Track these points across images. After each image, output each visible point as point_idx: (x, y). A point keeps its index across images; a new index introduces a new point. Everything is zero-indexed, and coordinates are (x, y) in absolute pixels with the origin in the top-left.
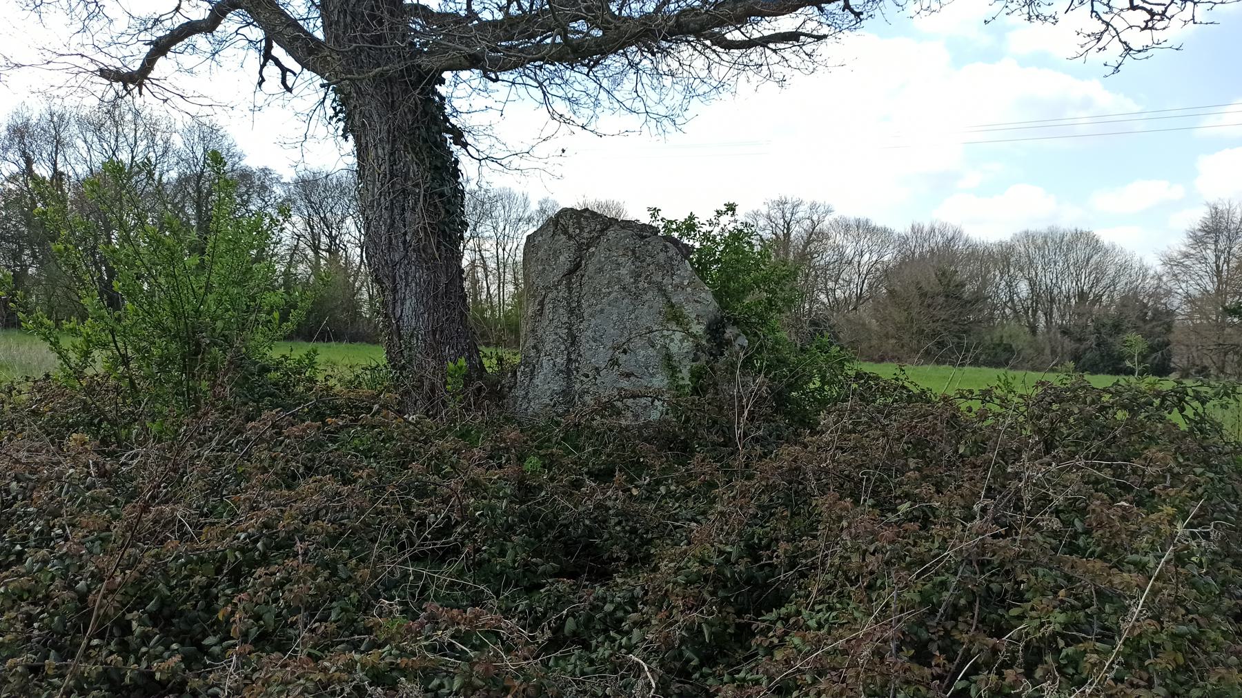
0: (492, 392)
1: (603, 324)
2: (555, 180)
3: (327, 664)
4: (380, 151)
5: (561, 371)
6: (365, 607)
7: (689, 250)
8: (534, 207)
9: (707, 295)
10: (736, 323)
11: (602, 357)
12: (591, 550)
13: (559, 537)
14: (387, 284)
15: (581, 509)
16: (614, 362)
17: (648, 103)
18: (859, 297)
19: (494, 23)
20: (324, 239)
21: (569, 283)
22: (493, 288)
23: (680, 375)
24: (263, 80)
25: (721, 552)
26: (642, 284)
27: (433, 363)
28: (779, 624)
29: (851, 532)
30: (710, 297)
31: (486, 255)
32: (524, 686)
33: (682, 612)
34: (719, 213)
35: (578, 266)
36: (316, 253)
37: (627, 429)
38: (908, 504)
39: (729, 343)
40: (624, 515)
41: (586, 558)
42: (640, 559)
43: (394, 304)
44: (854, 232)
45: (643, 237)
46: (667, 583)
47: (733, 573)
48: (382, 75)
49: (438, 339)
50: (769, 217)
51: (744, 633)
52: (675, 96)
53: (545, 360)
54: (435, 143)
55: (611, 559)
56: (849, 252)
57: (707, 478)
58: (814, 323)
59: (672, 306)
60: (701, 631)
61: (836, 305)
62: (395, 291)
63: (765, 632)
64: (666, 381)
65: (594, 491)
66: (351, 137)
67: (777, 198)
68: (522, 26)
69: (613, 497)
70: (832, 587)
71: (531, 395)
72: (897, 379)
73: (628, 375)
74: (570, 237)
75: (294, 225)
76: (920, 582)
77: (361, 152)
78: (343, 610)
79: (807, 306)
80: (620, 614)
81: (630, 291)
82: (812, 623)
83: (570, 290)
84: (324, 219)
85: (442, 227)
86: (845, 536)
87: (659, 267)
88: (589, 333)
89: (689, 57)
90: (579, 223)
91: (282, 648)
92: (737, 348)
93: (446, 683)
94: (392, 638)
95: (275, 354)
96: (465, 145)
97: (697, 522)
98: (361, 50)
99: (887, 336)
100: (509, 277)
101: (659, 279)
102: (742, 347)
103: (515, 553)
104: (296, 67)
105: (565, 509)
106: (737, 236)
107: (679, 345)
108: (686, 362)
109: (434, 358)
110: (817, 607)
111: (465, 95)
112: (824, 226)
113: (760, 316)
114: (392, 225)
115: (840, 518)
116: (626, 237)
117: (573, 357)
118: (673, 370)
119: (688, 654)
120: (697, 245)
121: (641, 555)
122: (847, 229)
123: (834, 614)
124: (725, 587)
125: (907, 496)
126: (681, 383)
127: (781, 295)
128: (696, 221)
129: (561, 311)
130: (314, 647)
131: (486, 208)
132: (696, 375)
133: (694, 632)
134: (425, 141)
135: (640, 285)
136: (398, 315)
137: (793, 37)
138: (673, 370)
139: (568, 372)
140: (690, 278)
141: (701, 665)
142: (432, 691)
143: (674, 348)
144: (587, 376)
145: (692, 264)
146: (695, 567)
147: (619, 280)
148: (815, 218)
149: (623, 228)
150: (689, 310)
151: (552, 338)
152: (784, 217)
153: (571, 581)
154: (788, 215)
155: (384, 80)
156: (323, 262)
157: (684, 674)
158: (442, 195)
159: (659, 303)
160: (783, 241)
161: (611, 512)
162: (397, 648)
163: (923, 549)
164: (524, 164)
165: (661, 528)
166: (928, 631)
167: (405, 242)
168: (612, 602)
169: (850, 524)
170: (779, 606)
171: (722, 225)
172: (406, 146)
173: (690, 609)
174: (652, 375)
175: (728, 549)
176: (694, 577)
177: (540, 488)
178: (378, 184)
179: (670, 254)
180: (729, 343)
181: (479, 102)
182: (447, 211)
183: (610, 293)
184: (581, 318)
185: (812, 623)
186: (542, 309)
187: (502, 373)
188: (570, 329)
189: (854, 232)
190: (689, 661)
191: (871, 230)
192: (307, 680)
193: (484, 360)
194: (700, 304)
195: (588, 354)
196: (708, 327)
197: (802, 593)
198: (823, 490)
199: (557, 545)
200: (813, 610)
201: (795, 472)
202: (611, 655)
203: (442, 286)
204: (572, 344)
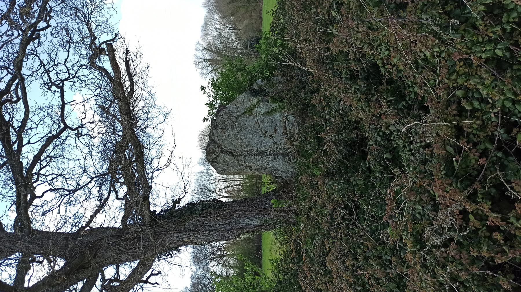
0: (284, 188)
1: (254, 141)
2: (192, 161)
3: (412, 263)
4: (185, 236)
5: (275, 158)
6: (384, 244)
7: (221, 105)
8: (203, 168)
9: (240, 97)
10: (252, 85)
11: (268, 141)
12: (353, 145)
13: (347, 159)
14: (240, 231)
15: (336, 151)
16: (271, 136)
17: (158, 122)
18: (235, 29)
19: (129, 188)
20: (219, 253)
21: (237, 156)
22: (236, 183)
23: (275, 108)
24: (156, 283)
25: (355, 92)
26: (237, 125)
27: (273, 211)
28: (387, 67)
29: (346, 37)
30: (241, 96)
31: (223, 186)
32: (419, 179)
33: (382, 109)
34: (205, 93)
35: (230, 152)
36: (225, 256)
37: (299, 131)
38: (333, 12)
39: (260, 87)
40: (339, 132)
41: (357, 148)
42: (357, 125)
43: (249, 228)
44: (207, 32)
45: (217, 125)
46: (369, 115)
47: (364, 87)
48: (154, 237)
49: (263, 210)
50: (202, 68)
51: (390, 82)
52: (154, 112)
53: (270, 165)
54: (181, 213)
55: (357, 137)
56: (215, 33)
57: (322, 98)
58: (246, 48)
59: (246, 112)
60: (390, 101)
61: (238, 39)
62: (243, 228)
63: (390, 73)
64: (278, 114)
65: (329, 146)
66: (180, 248)
67: (194, 65)
68: (129, 178)
69: (330, 137)
70: (370, 44)
71: (285, 170)
72: (273, 14)
73: (275, 130)
74: (218, 156)
75: (213, 266)
76: (368, 7)
77: (186, 244)
78: (386, 254)
79: (239, 51)
80: (381, 134)
81: (240, 130)
82: (387, 53)
83: (240, 155)
84: (211, 253)
85: (216, 210)
86: (350, 41)
87: (229, 118)
88: (258, 147)
89: (139, 106)
90: (212, 153)
91: (401, 278)
92: (262, 84)
93: (418, 211)
94: (398, 234)
95: (270, 275)
96: (180, 199)
97: (340, 101)
98: (143, 245)
99: (250, 16)
100: (232, 177)
101: (234, 118)
102: (262, 82)
103: (358, 180)
104: (151, 270)
105: (336, 158)
106: (214, 86)
107: (262, 109)
108: (269, 106)
109: (271, 211)
110: (379, 51)
111: (159, 202)
112: (204, 44)
113: (248, 74)
114: (216, 230)
115: (342, 42)
116: (217, 133)
117: (268, 153)
118: (273, 111)
119: (400, 106)
120: (219, 102)
121: (355, 125)
122: (206, 35)
123: (383, 44)
124: (369, 90)
125: (329, 12)
126: (278, 107)
127: (238, 66)
128: (208, 102)
129: (249, 159)
130: (403, 267)
131: (203, 189)
132: (274, 101)
133: (390, 104)
134: (180, 217)
135: (237, 126)
136: (253, 226)
137: (127, 63)
138: (273, 111)
139: (275, 155)
140: (233, 105)
141: (405, 100)
142: (422, 217)
143: (263, 111)
144: (277, 148)
145: (227, 104)
146: (362, 103)
147: (236, 135)
148: (202, 49)
149: (213, 134)
150: (247, 105)
151: (259, 162)
152: (202, 62)
153: (369, 156)
154: (201, 60)
155: (156, 235)
156: (228, 253)
157: (410, 108)
158: (202, 210)
159: (244, 117)
160: (212, 62)
161: (337, 138)
162: (403, 232)
163: (354, 6)
164: (186, 174)
165: (343, 117)
166: (391, 4)
167: (223, 225)
168: (377, 138)
169: (344, 39)
170: (379, 67)
171: (210, 91)
172: (182, 226)
173: (381, 105)
174: (275, 119)
175: (353, 89)
176: (366, 104)
177: (327, 168)
178: (199, 236)
179: (224, 114)
180: (260, 87)
181: (162, 194)
182: (209, 207)
183: (241, 139)
184: (252, 150)
185: (387, 53)
186: (248, 167)
187: (276, 182)
188: (257, 155)
189: (207, 32)
190: (403, 106)
191: (206, 24)
192: (420, 272)
193: (271, 190)
194: (244, 100)
195: (267, 147)
196: (254, 96)
197: (372, 57)
198: (329, 49)
199: (350, 159)
200: (380, 53)
201: (320, 61)
202: (402, 139)
203: (241, 209)
204: (263, 154)
